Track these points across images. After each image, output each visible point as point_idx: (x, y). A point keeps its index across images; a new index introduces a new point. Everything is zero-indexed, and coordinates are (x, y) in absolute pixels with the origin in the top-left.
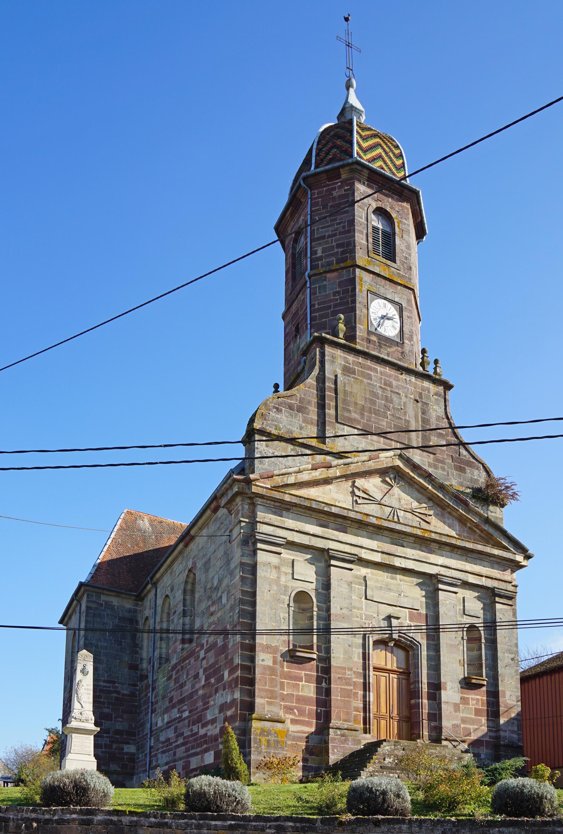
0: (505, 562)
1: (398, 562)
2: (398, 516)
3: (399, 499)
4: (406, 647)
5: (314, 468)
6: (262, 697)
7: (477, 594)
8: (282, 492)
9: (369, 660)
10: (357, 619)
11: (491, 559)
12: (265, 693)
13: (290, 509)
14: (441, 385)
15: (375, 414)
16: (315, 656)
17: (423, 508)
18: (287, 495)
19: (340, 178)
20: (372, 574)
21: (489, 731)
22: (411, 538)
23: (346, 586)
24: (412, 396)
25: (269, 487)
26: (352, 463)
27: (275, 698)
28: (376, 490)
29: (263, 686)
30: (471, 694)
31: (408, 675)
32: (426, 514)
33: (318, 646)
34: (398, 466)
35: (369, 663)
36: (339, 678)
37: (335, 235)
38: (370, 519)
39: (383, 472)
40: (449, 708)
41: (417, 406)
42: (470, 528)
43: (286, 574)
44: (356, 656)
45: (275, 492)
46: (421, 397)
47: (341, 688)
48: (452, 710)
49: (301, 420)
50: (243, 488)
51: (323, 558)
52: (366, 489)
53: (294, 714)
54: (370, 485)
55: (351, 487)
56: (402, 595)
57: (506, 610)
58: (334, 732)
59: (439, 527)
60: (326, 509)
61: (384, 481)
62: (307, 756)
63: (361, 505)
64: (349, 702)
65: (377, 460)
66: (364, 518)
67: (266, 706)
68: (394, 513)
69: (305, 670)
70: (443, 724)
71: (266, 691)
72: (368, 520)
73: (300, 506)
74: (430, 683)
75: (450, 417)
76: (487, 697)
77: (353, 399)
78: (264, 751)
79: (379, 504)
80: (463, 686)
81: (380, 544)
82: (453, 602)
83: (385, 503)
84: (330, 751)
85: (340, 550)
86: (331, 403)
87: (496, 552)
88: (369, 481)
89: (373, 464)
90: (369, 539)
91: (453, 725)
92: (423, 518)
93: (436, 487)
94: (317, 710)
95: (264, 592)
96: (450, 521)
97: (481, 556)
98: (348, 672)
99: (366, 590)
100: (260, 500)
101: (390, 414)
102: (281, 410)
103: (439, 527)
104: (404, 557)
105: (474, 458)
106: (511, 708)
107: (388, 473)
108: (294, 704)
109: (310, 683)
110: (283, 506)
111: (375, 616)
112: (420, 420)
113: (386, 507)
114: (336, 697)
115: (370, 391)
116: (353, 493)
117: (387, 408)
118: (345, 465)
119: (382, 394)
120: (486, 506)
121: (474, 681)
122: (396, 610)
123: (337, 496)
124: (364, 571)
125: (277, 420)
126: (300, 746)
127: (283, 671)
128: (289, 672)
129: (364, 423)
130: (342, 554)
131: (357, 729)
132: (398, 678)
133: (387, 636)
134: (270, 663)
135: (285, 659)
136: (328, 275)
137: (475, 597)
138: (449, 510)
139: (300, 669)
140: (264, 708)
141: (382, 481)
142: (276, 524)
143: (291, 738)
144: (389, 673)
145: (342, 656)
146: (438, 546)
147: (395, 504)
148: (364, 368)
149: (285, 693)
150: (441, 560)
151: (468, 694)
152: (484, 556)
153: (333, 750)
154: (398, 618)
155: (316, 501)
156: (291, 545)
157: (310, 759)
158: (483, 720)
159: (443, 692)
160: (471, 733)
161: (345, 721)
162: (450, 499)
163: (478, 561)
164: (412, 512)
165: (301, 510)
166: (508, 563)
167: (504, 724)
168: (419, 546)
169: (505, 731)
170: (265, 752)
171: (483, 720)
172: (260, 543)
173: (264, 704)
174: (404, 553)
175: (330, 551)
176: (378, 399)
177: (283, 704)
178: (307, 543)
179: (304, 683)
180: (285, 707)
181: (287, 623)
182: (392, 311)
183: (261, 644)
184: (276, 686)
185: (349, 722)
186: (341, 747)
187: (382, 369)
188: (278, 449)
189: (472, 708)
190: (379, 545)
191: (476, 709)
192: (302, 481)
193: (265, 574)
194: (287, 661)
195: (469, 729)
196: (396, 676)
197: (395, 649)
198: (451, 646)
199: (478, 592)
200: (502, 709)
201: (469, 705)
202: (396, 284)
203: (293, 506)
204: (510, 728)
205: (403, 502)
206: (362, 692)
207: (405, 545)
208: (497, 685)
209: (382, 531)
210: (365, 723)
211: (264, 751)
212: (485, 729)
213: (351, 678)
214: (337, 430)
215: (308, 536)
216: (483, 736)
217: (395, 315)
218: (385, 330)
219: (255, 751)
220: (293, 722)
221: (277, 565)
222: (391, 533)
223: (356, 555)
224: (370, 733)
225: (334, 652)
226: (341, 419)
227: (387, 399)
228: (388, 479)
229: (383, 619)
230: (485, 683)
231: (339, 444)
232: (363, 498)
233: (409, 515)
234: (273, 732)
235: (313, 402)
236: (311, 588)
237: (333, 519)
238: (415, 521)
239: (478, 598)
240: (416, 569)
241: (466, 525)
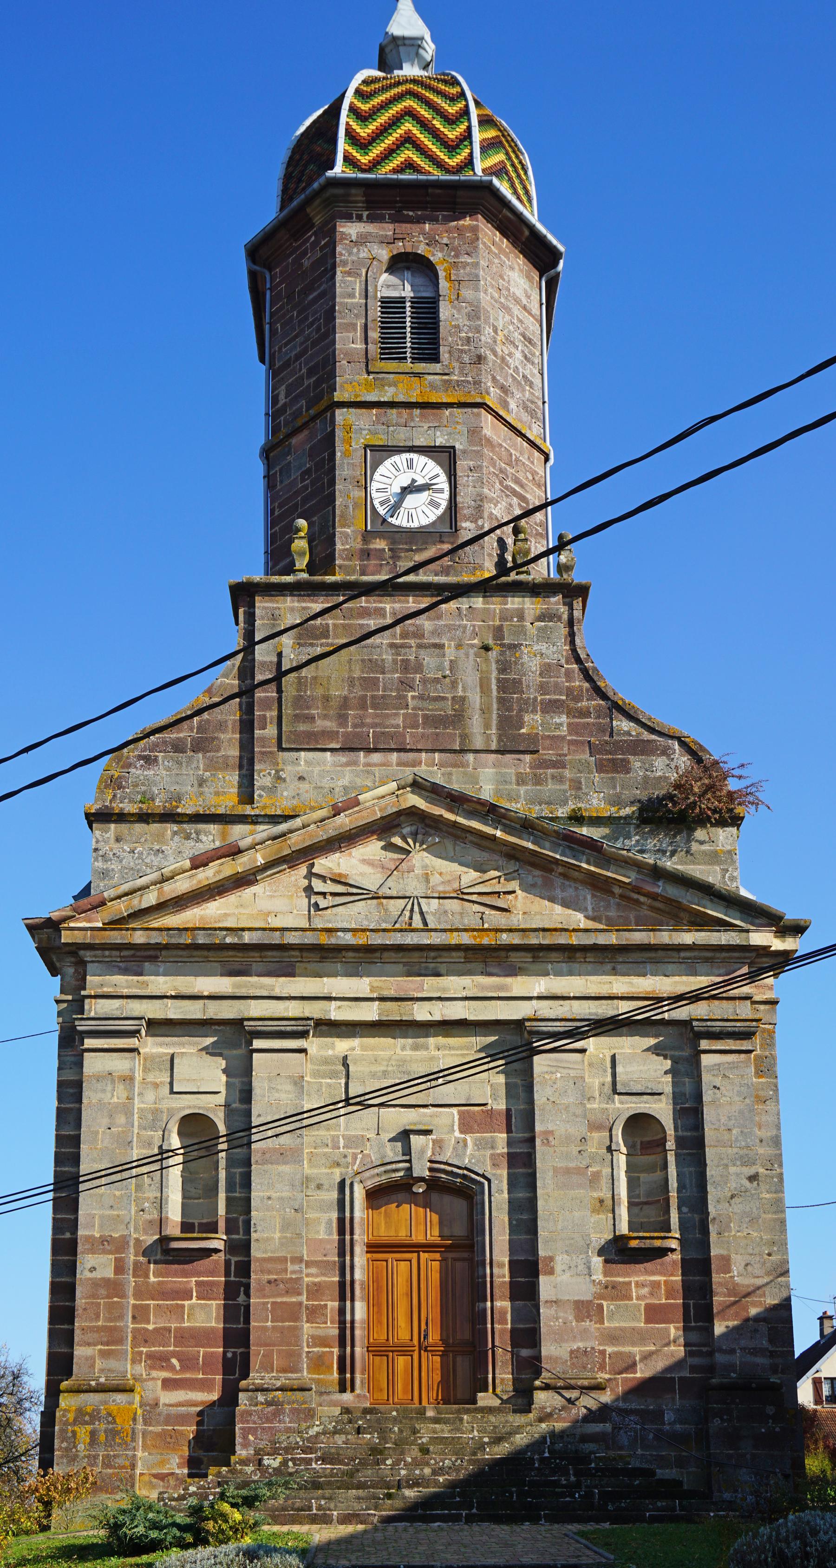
0: (724, 954)
1: (421, 1013)
2: (422, 913)
3: (427, 878)
4: (454, 1191)
5: (199, 863)
7: (652, 1041)
8: (127, 929)
9: (352, 1233)
10: (326, 1150)
11: (683, 954)
12: (96, 1335)
13: (157, 957)
14: (554, 594)
15: (374, 707)
16: (219, 1245)
17: (493, 880)
18: (139, 933)
19: (313, 226)
20: (363, 1048)
21: (689, 1354)
22: (454, 954)
23: (289, 1087)
24: (476, 641)
25: (100, 925)
26: (291, 831)
28: (368, 869)
29: (91, 1320)
30: (636, 1273)
31: (463, 1250)
32: (499, 893)
33: (228, 1221)
34: (414, 806)
35: (352, 1240)
36: (269, 1282)
38: (338, 937)
39: (384, 827)
40: (561, 1314)
41: (487, 660)
42: (622, 896)
43: (156, 1086)
44: (322, 1228)
45: (112, 933)
46: (498, 632)
47: (273, 1303)
48: (571, 1318)
49: (201, 766)
50: (49, 938)
51: (235, 1039)
52: (340, 875)
53: (172, 1368)
54: (354, 861)
55: (305, 877)
57: (733, 1066)
58: (250, 1399)
59: (534, 912)
60: (228, 940)
61: (390, 847)
62: (201, 1453)
63: (329, 911)
65: (356, 809)
66: (324, 939)
67: (97, 1361)
68: (412, 910)
69: (199, 1274)
70: (544, 1352)
71: (99, 1329)
72: (333, 941)
73: (167, 947)
74: (518, 1261)
75: (583, 656)
76: (683, 1275)
77: (320, 692)
78: (82, 1454)
79: (373, 898)
80: (613, 1257)
81: (377, 981)
82: (573, 1073)
83: (389, 893)
84: (238, 1440)
86: (268, 714)
87: (688, 938)
88: (350, 854)
89: (347, 820)
90: (351, 976)
91: (572, 1352)
92: (492, 902)
93: (515, 829)
94: (224, 1353)
95: (98, 1132)
96: (570, 892)
97: (652, 954)
98: (290, 1267)
99: (347, 1084)
100: (88, 953)
101: (413, 697)
102: (156, 759)
103: (536, 914)
104: (440, 999)
105: (652, 730)
106: (748, 1295)
107: (398, 825)
108: (172, 1348)
109: (210, 1299)
110: (138, 954)
111: (372, 1135)
112: (494, 687)
113: (392, 901)
114: (261, 1324)
115: (363, 661)
116: (309, 890)
117: (406, 684)
118: (274, 838)
119: (393, 660)
120: (684, 834)
121: (634, 1244)
122: (425, 1115)
123: (274, 906)
124: (342, 1046)
125: (148, 782)
126: (181, 1433)
127: (148, 1283)
128: (159, 1283)
129: (346, 735)
130: (276, 1023)
131: (308, 1386)
132: (443, 1260)
133: (401, 1174)
134: (109, 1273)
135: (152, 1259)
136: (294, 441)
137: (648, 1050)
138: (561, 869)
139: (186, 1274)
140: (93, 1366)
141: (384, 848)
142: (125, 992)
143: (162, 1418)
144: (418, 1252)
145: (277, 1235)
146: (530, 955)
147: (414, 887)
148: (352, 617)
149: (151, 1327)
150: (540, 985)
152: (660, 953)
153: (245, 1438)
154: (428, 1132)
155: (204, 929)
156: (159, 1027)
157: (205, 1459)
158: (673, 1331)
159: (542, 1279)
160: (634, 1364)
161: (284, 1370)
162: (554, 848)
163: (648, 966)
164: (461, 895)
165: (180, 953)
166: (736, 955)
167: (723, 1335)
168: (482, 965)
169: (732, 1351)
170: (85, 1456)
171: (673, 1331)
173: (93, 1358)
174: (438, 990)
175: (246, 1023)
176: (383, 673)
177: (145, 1350)
178: (199, 1016)
179: (194, 1300)
180: (150, 1356)
181: (159, 1185)
182: (427, 469)
183: (89, 1239)
185: (292, 1372)
186: (263, 1429)
187: (397, 606)
188: (143, 840)
190: (375, 984)
191: (648, 1307)
192: (174, 895)
193: (100, 1095)
194: (155, 1263)
195: (630, 1355)
196: (437, 1256)
197: (435, 1196)
198: (568, 1171)
199: (656, 1036)
200: (718, 1300)
201: (631, 1299)
202: (439, 408)
203: (161, 949)
204: (743, 1343)
205: (435, 879)
206: (336, 1304)
207: (443, 971)
208: (705, 1245)
209: (378, 954)
210: (342, 1370)
211: (82, 1454)
212: (678, 1351)
213: (299, 1279)
214: (280, 766)
215: (201, 1002)
216: (669, 1369)
217: (437, 476)
218: (410, 517)
219: (62, 1457)
220: (168, 1384)
221: (127, 1073)
222: (401, 955)
223: (308, 1019)
224: (353, 1390)
225: (259, 1228)
226: (288, 741)
227: (406, 666)
228: (397, 840)
229: (389, 1141)
230: (674, 1244)
231: (285, 794)
233: (453, 905)
234: (103, 1413)
235: (230, 724)
236: (214, 1106)
237: (257, 955)
238: (470, 915)
239: (656, 1050)
240: (472, 1017)
241: (613, 893)
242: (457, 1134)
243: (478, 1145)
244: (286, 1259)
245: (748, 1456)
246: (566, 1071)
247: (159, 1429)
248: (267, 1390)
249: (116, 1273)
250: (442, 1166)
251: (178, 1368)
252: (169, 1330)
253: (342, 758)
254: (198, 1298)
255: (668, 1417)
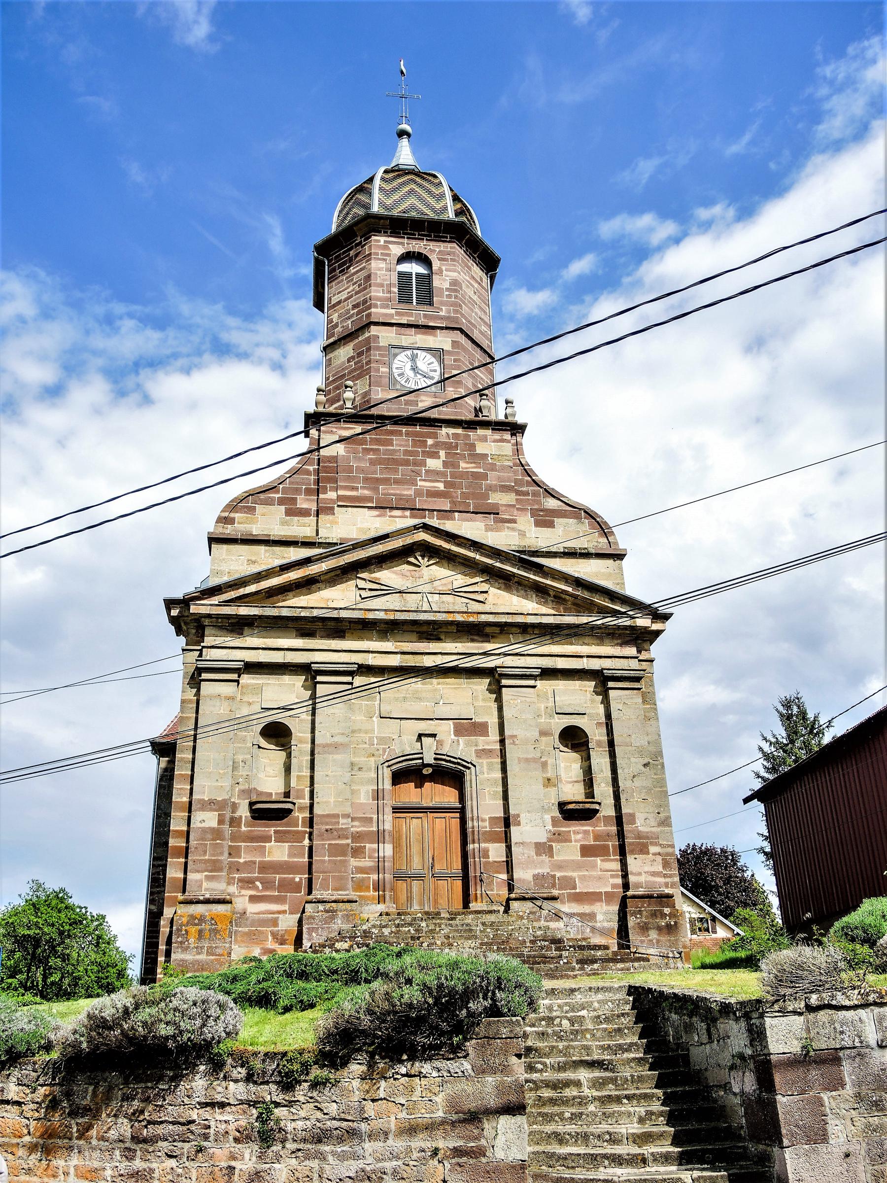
1: (428, 662)
6: (198, 871)
27: (220, 870)
29: (200, 856)
36: (327, 831)
37: (351, 296)
47: (329, 844)
56: (441, 703)
60: (303, 614)
64: (344, 862)
85: (339, 661)
91: (534, 876)
98: (341, 821)
111: (395, 737)
122: (431, 725)
134: (214, 824)
140: (200, 886)
145: (332, 800)
149: (242, 860)
151: (569, 826)
164: (454, 592)
169: (640, 874)
172: (205, 672)
180: (240, 880)
184: (222, 854)
185: (341, 890)
189: (575, 846)
198: (527, 760)
204: (646, 869)
215: (282, 652)
220: (253, 899)
225: (319, 795)
232: (370, 590)
234: (208, 918)
238: (459, 604)
242: (453, 737)
243: (467, 744)
244: (338, 815)
245: (654, 941)
246: (524, 699)
247: (247, 929)
248: (325, 902)
249: (219, 824)
250: (444, 757)
251: (261, 888)
252: (254, 863)
253: (375, 512)
254: (276, 841)
255: (599, 917)
